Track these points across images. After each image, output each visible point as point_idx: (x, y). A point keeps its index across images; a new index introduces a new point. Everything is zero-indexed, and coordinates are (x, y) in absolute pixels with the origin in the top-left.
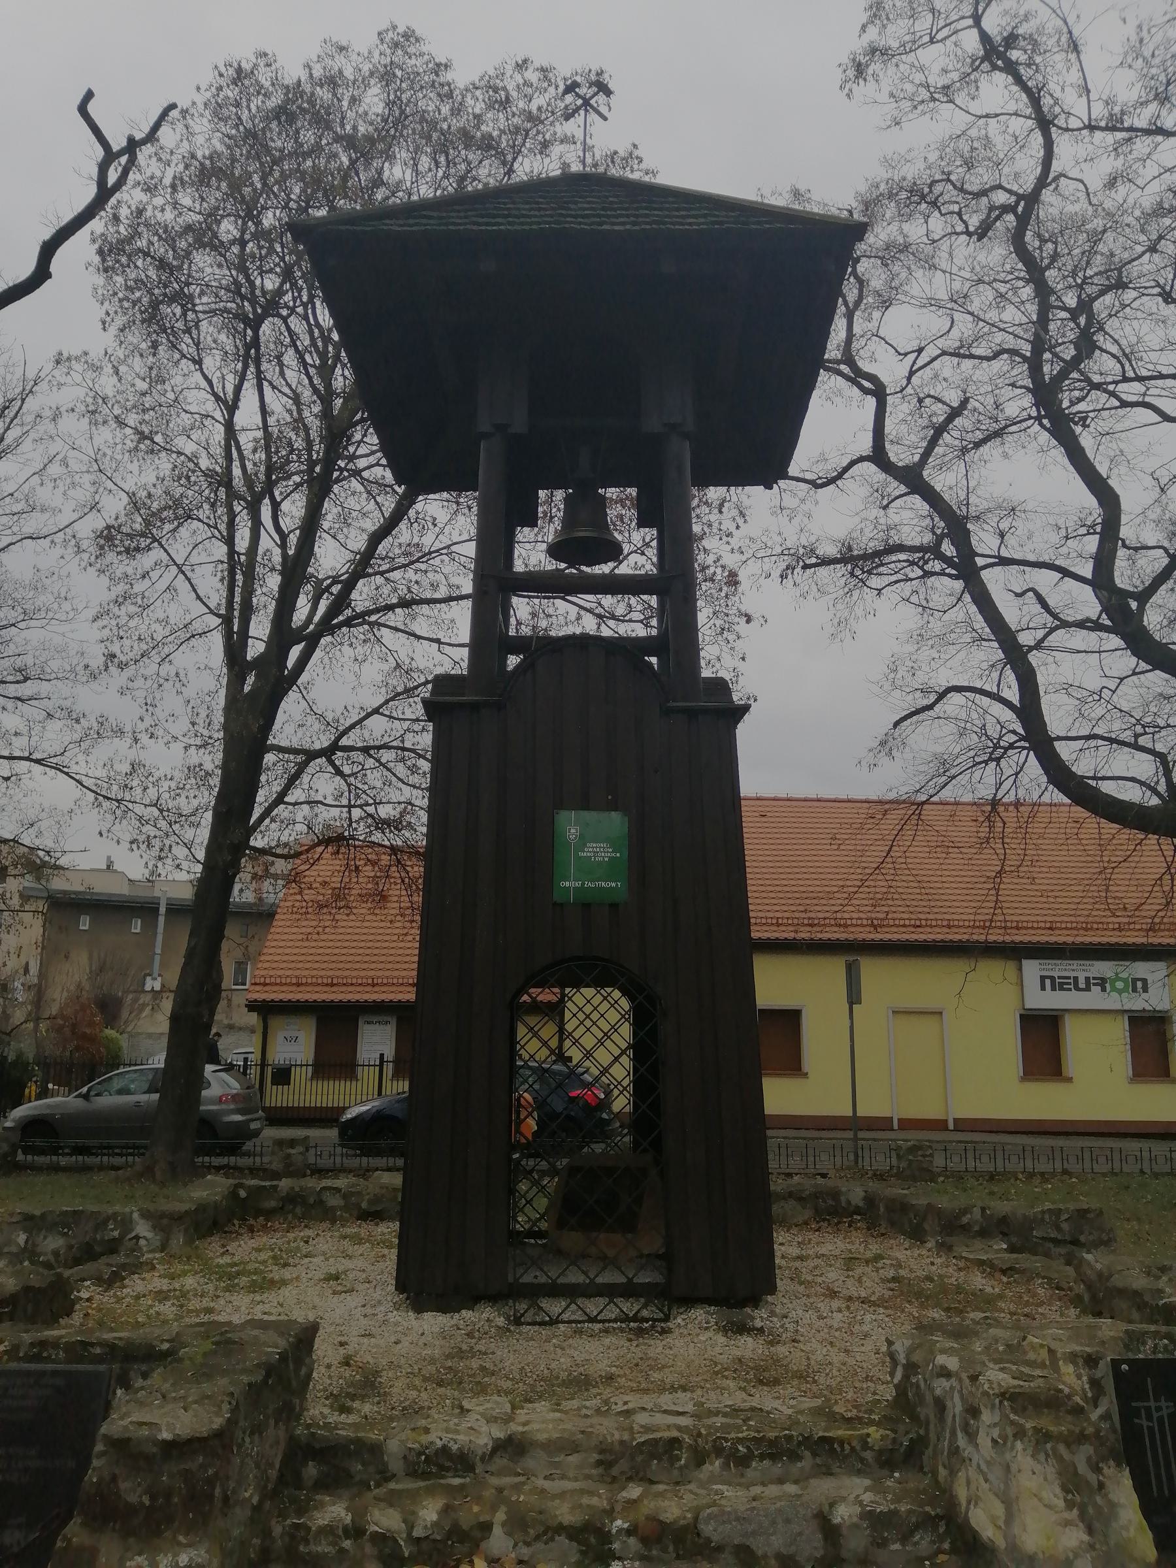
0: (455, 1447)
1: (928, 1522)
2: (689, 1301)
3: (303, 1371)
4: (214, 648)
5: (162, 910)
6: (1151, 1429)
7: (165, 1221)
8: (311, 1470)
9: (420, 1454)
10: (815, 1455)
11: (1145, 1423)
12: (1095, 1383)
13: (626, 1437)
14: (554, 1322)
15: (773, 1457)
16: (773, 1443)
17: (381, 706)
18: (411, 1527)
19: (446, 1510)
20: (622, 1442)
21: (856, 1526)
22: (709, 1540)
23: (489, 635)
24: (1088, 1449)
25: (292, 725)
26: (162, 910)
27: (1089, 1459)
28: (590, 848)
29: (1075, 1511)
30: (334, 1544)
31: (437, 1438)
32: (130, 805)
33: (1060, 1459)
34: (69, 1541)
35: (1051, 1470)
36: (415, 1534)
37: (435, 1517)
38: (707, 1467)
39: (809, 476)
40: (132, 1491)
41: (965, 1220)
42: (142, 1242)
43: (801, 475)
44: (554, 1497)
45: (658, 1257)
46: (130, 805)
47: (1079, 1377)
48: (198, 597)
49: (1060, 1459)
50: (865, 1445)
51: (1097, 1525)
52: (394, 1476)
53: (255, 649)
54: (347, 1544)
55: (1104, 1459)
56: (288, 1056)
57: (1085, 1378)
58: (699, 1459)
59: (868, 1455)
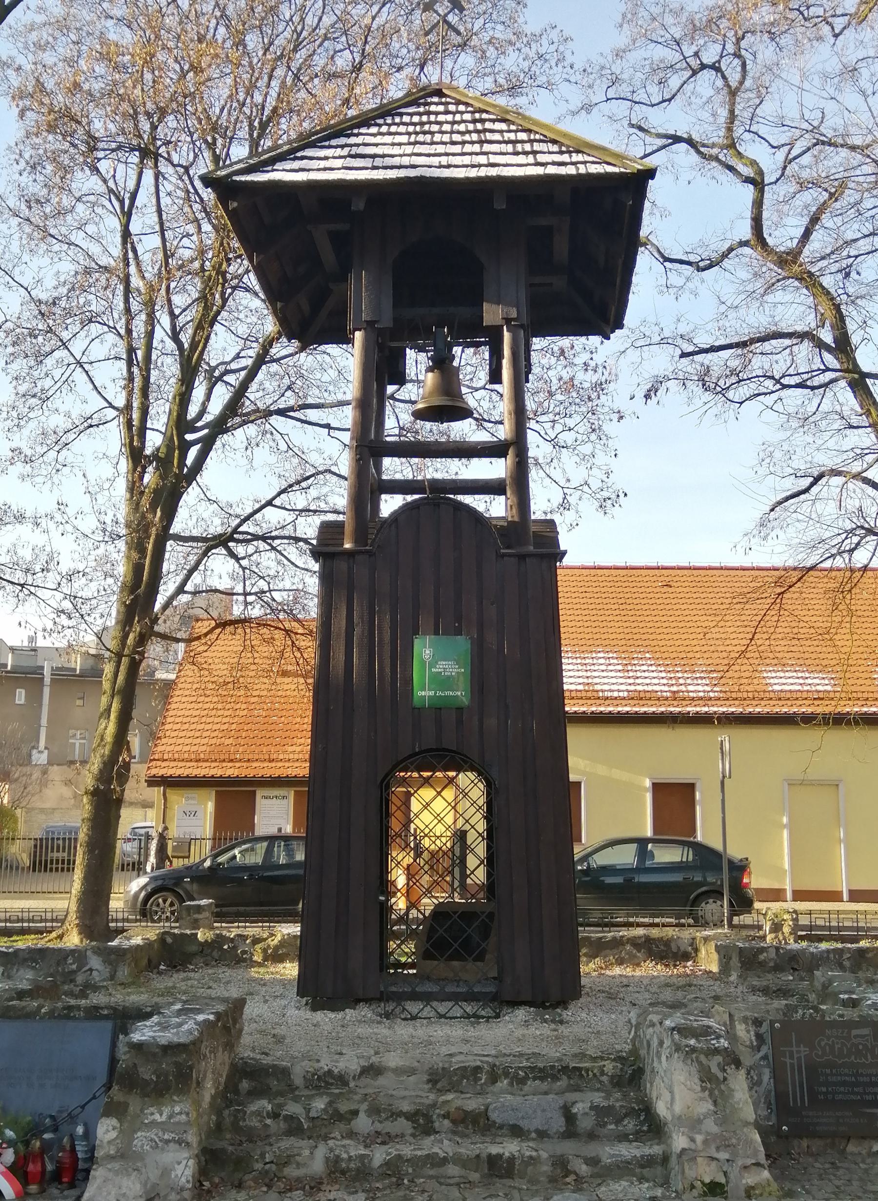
0: (336, 1071)
1: (631, 1113)
2: (515, 1004)
3: (237, 1026)
4: (113, 437)
5: (47, 680)
6: (792, 1065)
7: (113, 957)
8: (245, 1085)
9: (314, 1075)
10: (569, 1078)
11: (788, 1061)
12: (759, 1036)
13: (446, 1066)
14: (414, 1018)
15: (542, 1079)
16: (541, 1070)
17: (274, 498)
18: (308, 1111)
19: (330, 1103)
20: (443, 1069)
21: (586, 1114)
22: (494, 1122)
23: (367, 488)
24: (719, 1059)
25: (193, 515)
26: (47, 680)
27: (719, 1064)
28: (437, 668)
29: (707, 1093)
30: (261, 1121)
31: (325, 1064)
32: (32, 589)
33: (700, 1063)
34: (112, 1098)
35: (694, 1069)
36: (311, 1115)
37: (323, 1106)
38: (499, 1084)
39: (692, 258)
40: (146, 1073)
41: (761, 957)
42: (95, 973)
43: (684, 258)
44: (398, 1099)
45: (495, 978)
46: (32, 589)
47: (748, 1031)
48: (96, 388)
49: (700, 1063)
50: (603, 1073)
51: (719, 1101)
52: (297, 1088)
53: (154, 441)
54: (268, 1121)
55: (729, 1064)
56: (188, 830)
57: (752, 1033)
58: (494, 1078)
59: (605, 1079)
